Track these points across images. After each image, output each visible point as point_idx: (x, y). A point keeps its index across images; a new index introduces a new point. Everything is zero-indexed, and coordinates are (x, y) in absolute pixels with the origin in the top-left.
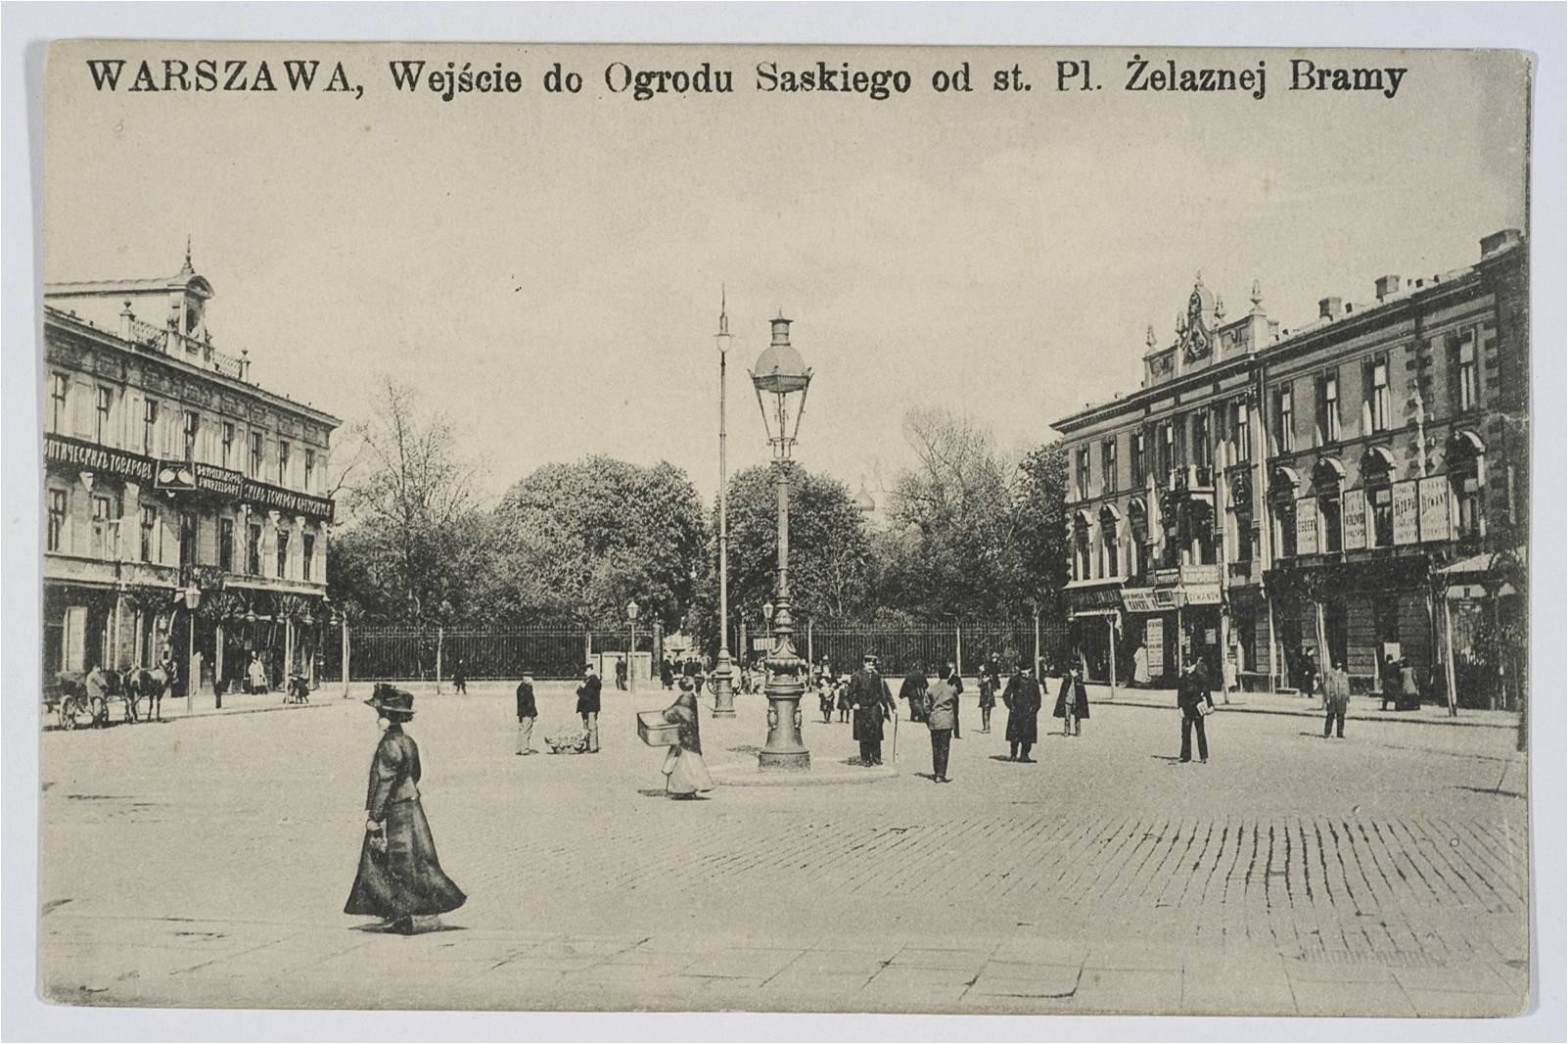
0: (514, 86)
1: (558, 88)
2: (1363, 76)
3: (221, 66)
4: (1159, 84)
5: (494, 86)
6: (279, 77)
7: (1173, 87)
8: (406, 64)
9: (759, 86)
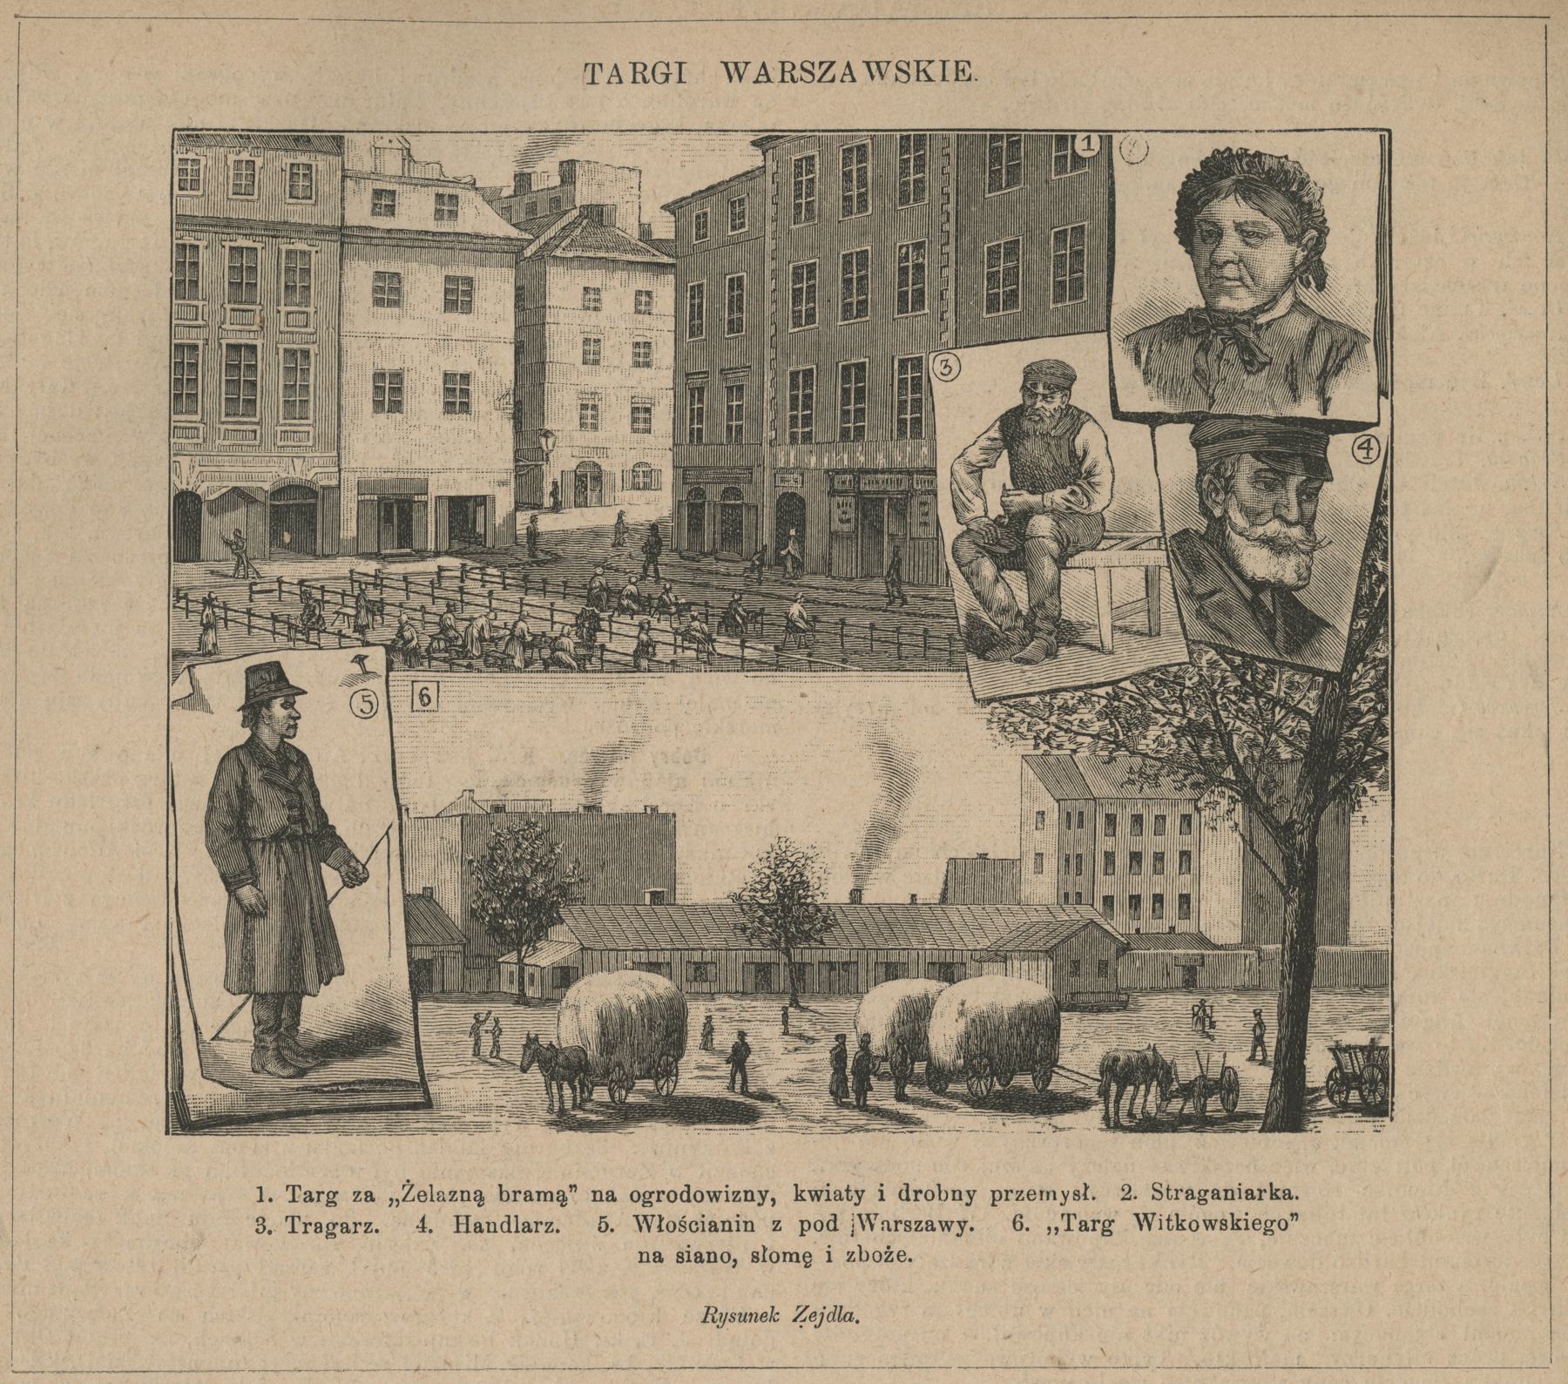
1: (689, 1200)
3: (817, 65)
6: (860, 71)
7: (432, 1200)
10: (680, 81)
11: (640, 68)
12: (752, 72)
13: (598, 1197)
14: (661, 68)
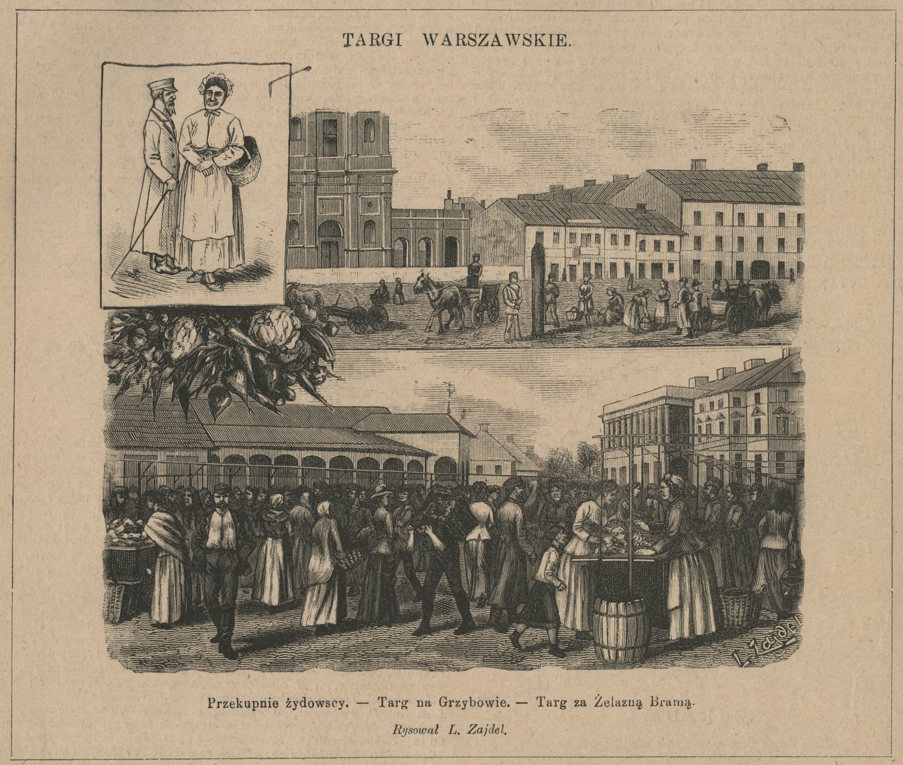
2: (264, 705)
3: (478, 36)
5: (611, 705)
6: (503, 40)
8: (490, 701)
9: (524, 44)
10: (398, 44)
11: (375, 37)
12: (439, 40)
13: (420, 704)
14: (387, 37)
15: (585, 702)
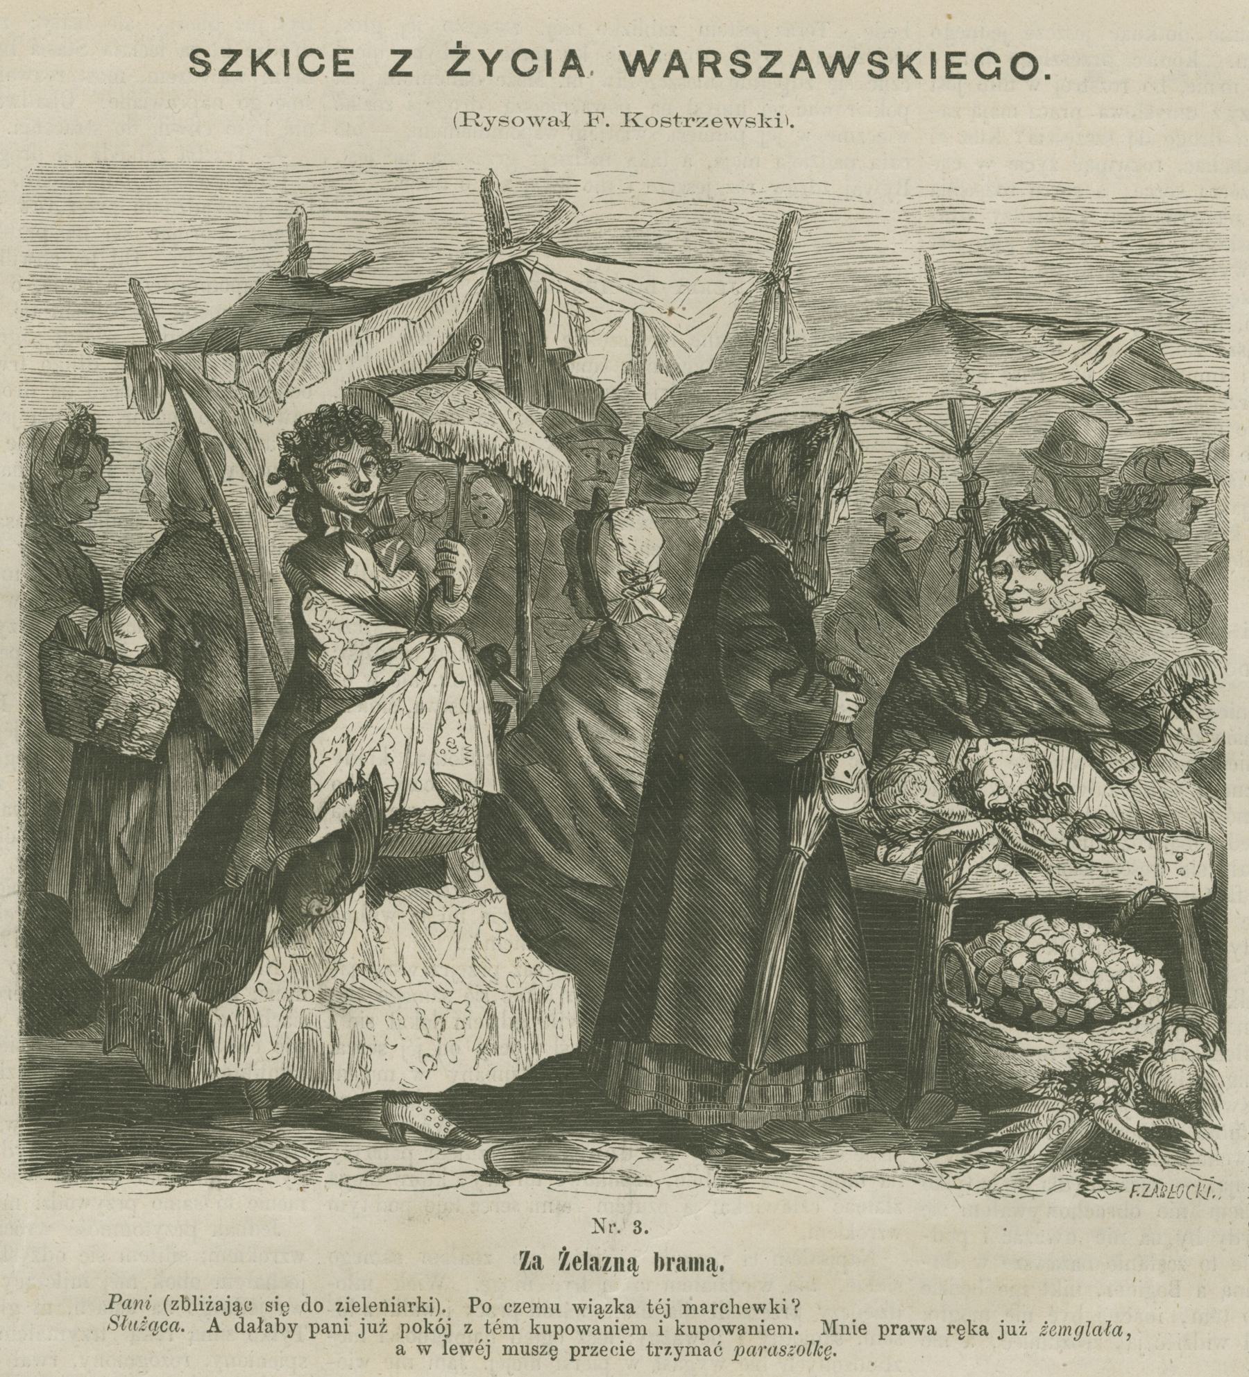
0: (863, 1331)
4: (373, 1309)
6: (692, 65)
15: (985, 1330)
